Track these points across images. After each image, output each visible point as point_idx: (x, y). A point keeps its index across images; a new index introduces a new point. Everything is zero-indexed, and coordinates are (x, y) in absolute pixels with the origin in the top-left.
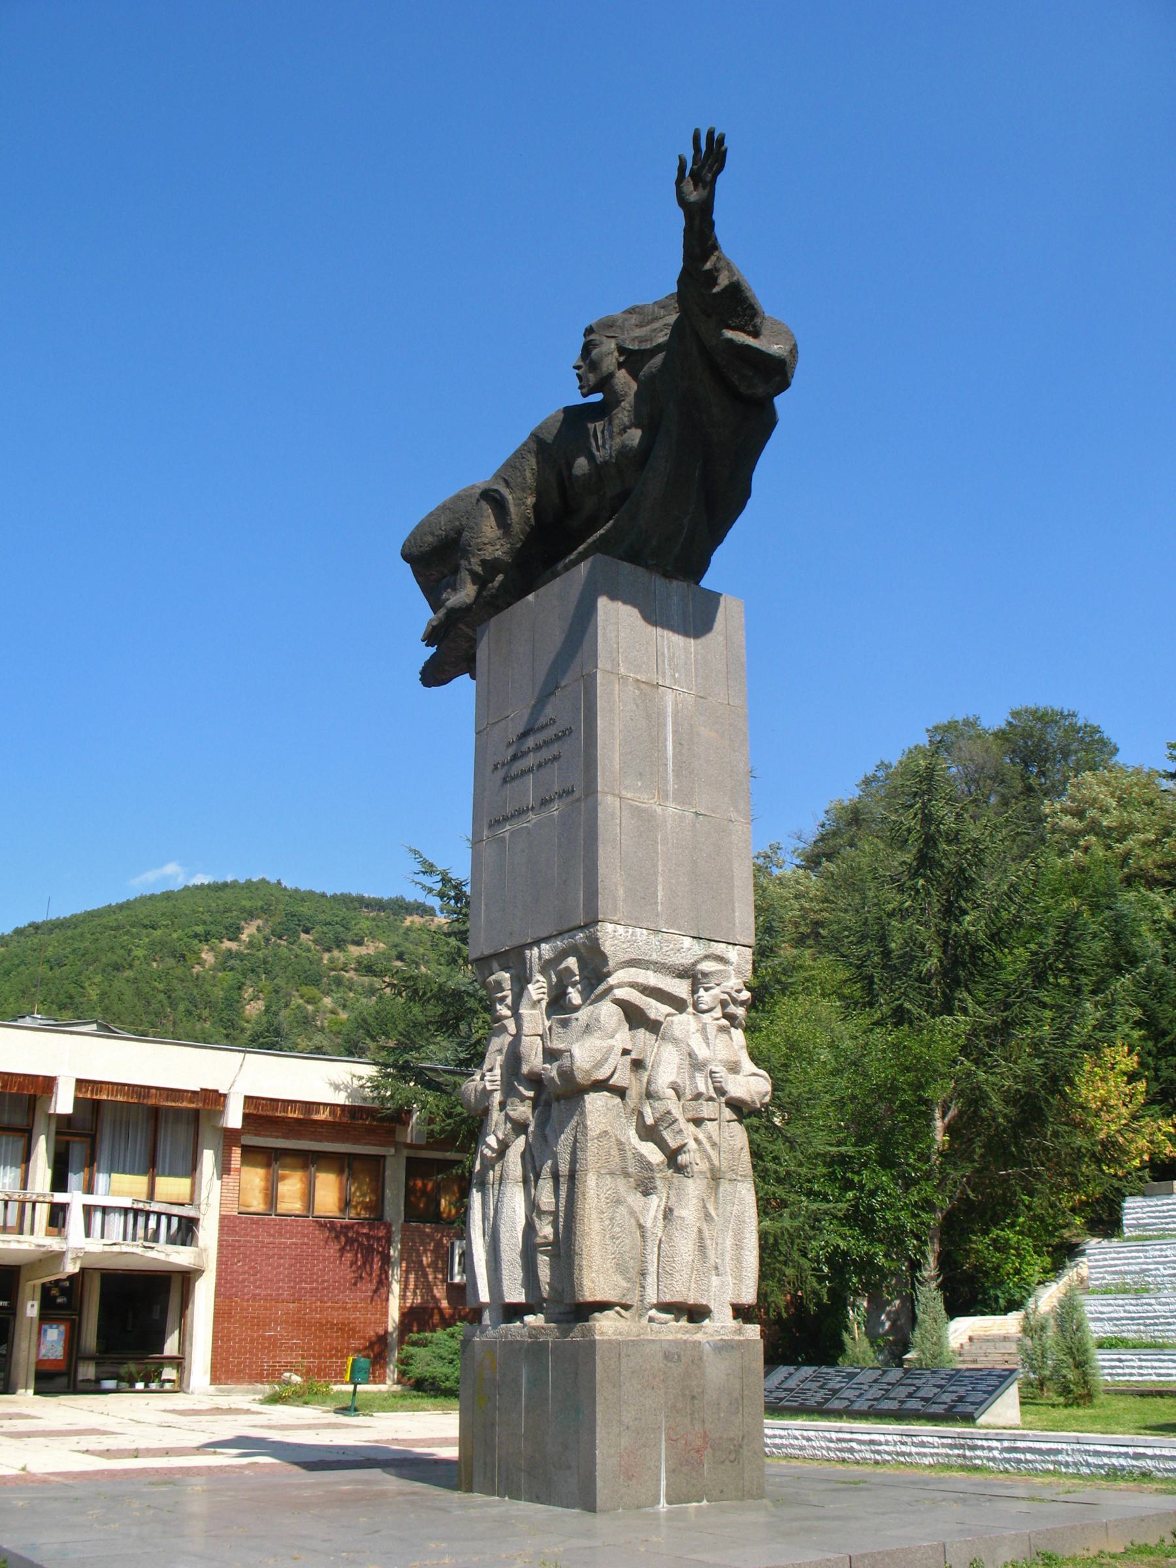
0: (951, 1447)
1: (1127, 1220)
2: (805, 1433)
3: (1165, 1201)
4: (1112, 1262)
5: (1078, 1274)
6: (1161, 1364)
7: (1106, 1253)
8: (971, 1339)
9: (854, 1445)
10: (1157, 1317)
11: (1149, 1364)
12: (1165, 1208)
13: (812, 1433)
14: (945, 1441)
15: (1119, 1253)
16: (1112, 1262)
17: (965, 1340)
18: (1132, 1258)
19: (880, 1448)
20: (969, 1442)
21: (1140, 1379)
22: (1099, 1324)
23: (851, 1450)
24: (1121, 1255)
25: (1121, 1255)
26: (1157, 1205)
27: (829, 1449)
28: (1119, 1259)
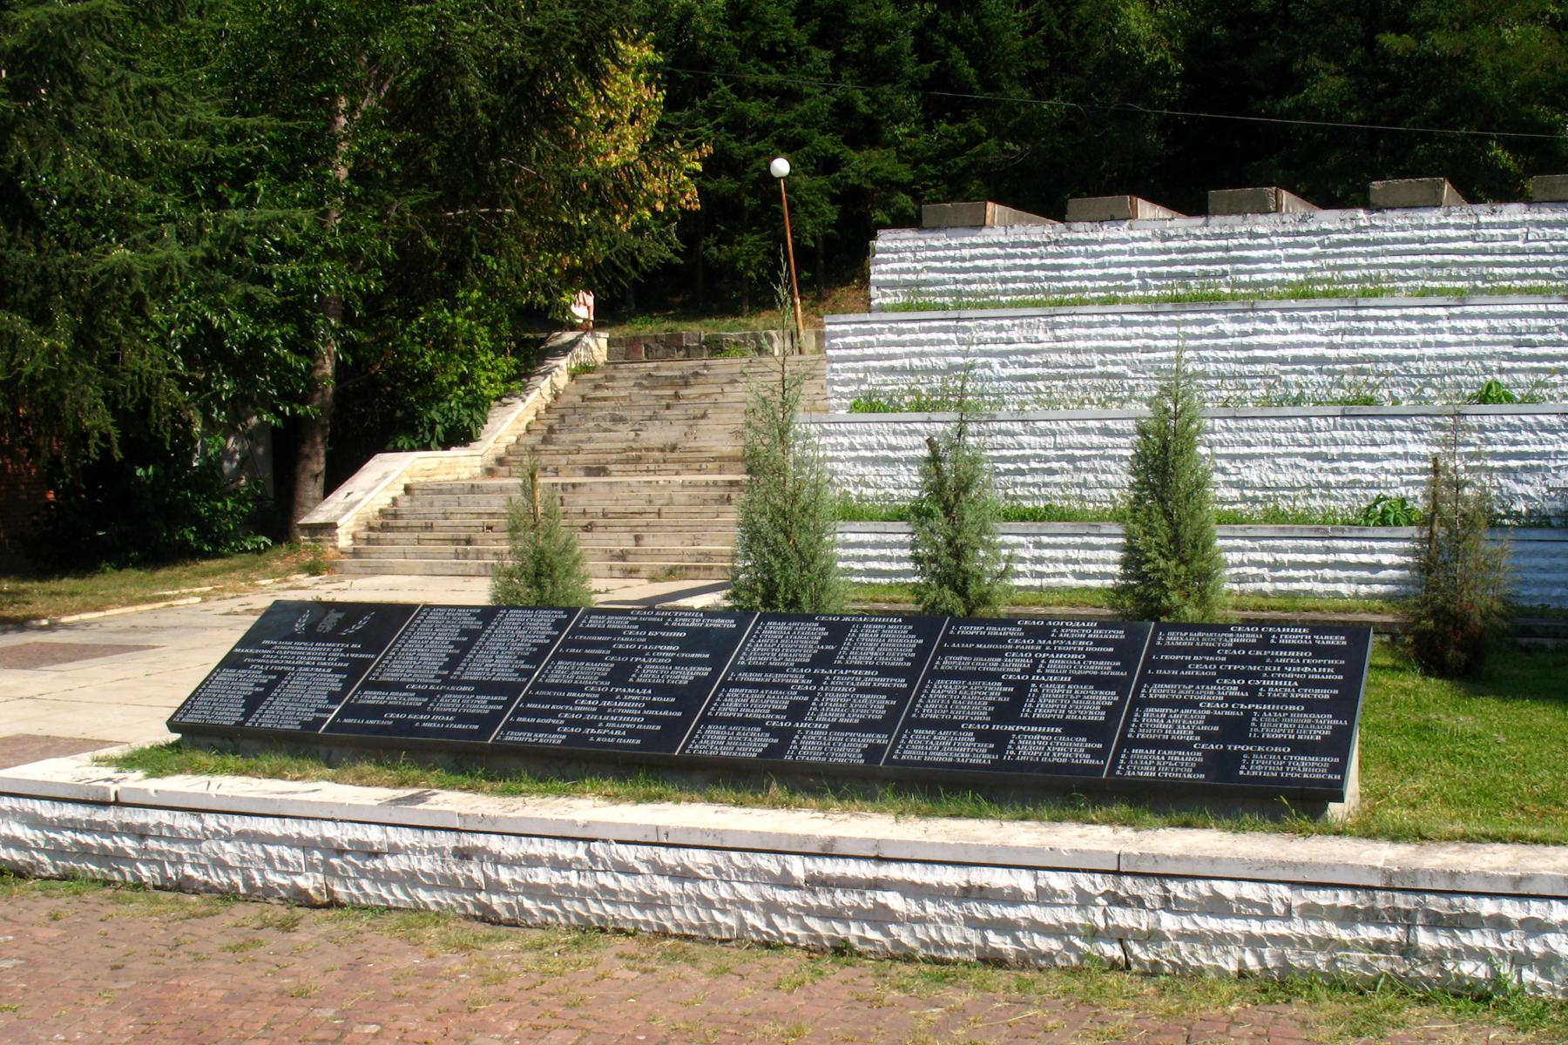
0: (1348, 917)
1: (879, 272)
2: (668, 857)
3: (967, 240)
4: (881, 350)
5: (553, 384)
6: (1089, 554)
7: (871, 332)
8: (408, 489)
9: (893, 900)
10: (1026, 459)
11: (1060, 554)
12: (966, 252)
13: (702, 857)
14: (1323, 898)
15: (901, 332)
16: (881, 350)
17: (399, 491)
18: (931, 343)
19: (1011, 913)
20: (1436, 904)
21: (1037, 583)
22: (883, 470)
23: (881, 917)
24: (906, 337)
25: (906, 337)
26: (948, 247)
27: (771, 907)
28: (903, 344)
